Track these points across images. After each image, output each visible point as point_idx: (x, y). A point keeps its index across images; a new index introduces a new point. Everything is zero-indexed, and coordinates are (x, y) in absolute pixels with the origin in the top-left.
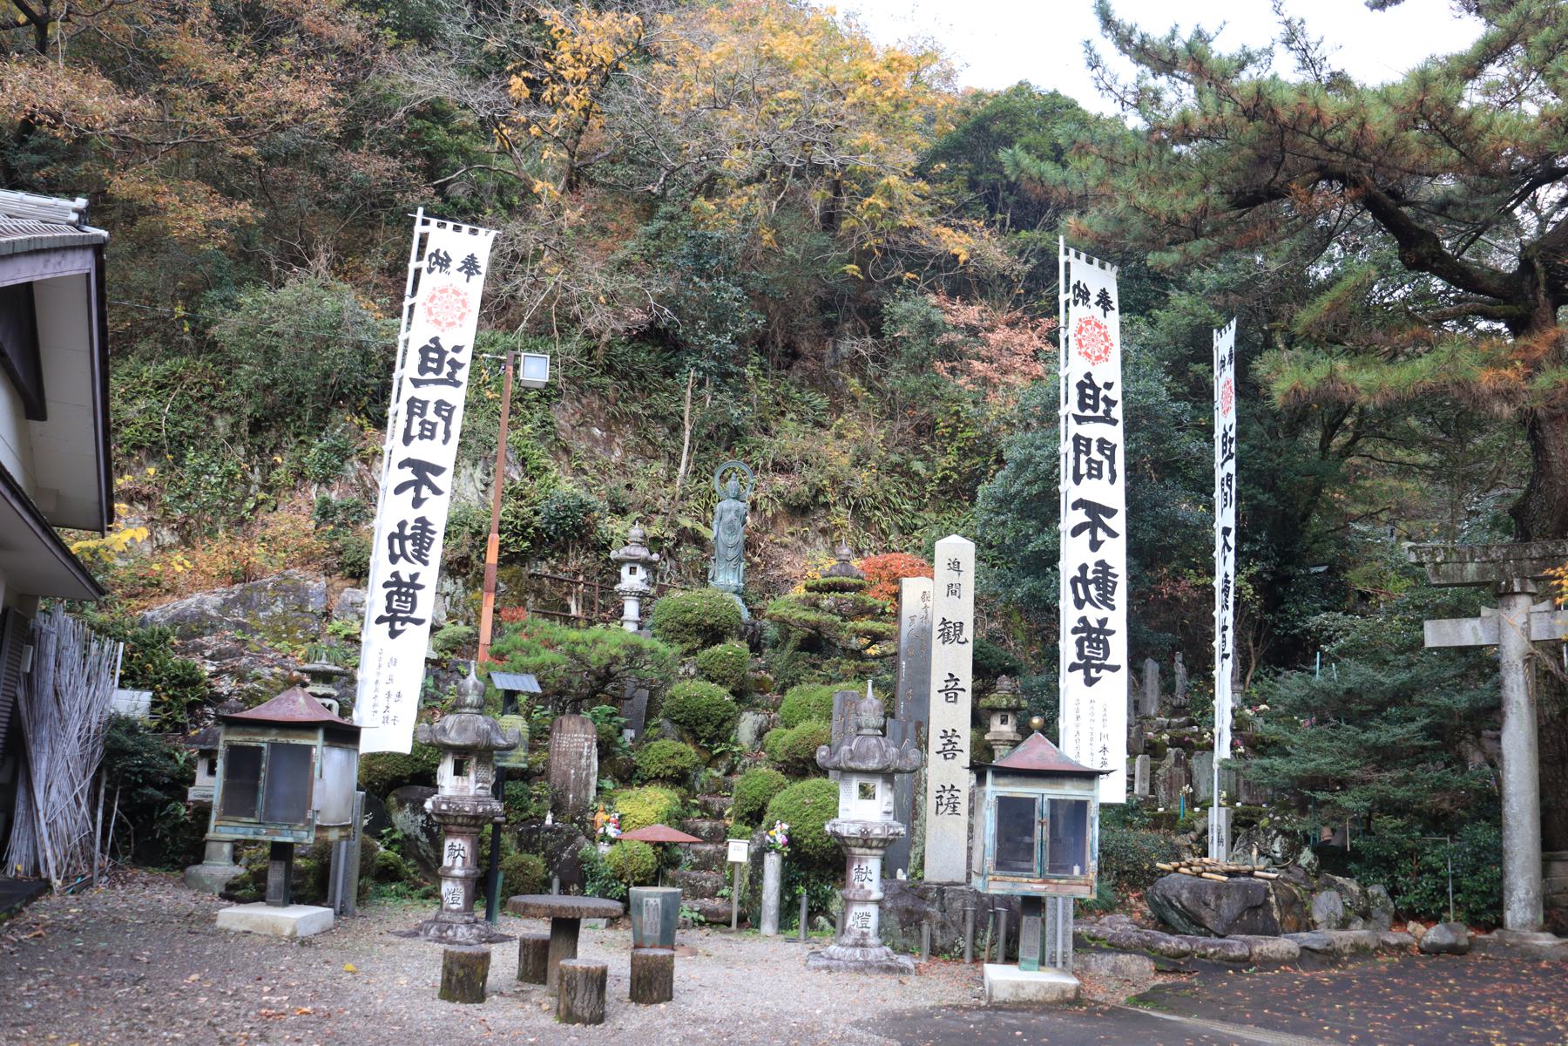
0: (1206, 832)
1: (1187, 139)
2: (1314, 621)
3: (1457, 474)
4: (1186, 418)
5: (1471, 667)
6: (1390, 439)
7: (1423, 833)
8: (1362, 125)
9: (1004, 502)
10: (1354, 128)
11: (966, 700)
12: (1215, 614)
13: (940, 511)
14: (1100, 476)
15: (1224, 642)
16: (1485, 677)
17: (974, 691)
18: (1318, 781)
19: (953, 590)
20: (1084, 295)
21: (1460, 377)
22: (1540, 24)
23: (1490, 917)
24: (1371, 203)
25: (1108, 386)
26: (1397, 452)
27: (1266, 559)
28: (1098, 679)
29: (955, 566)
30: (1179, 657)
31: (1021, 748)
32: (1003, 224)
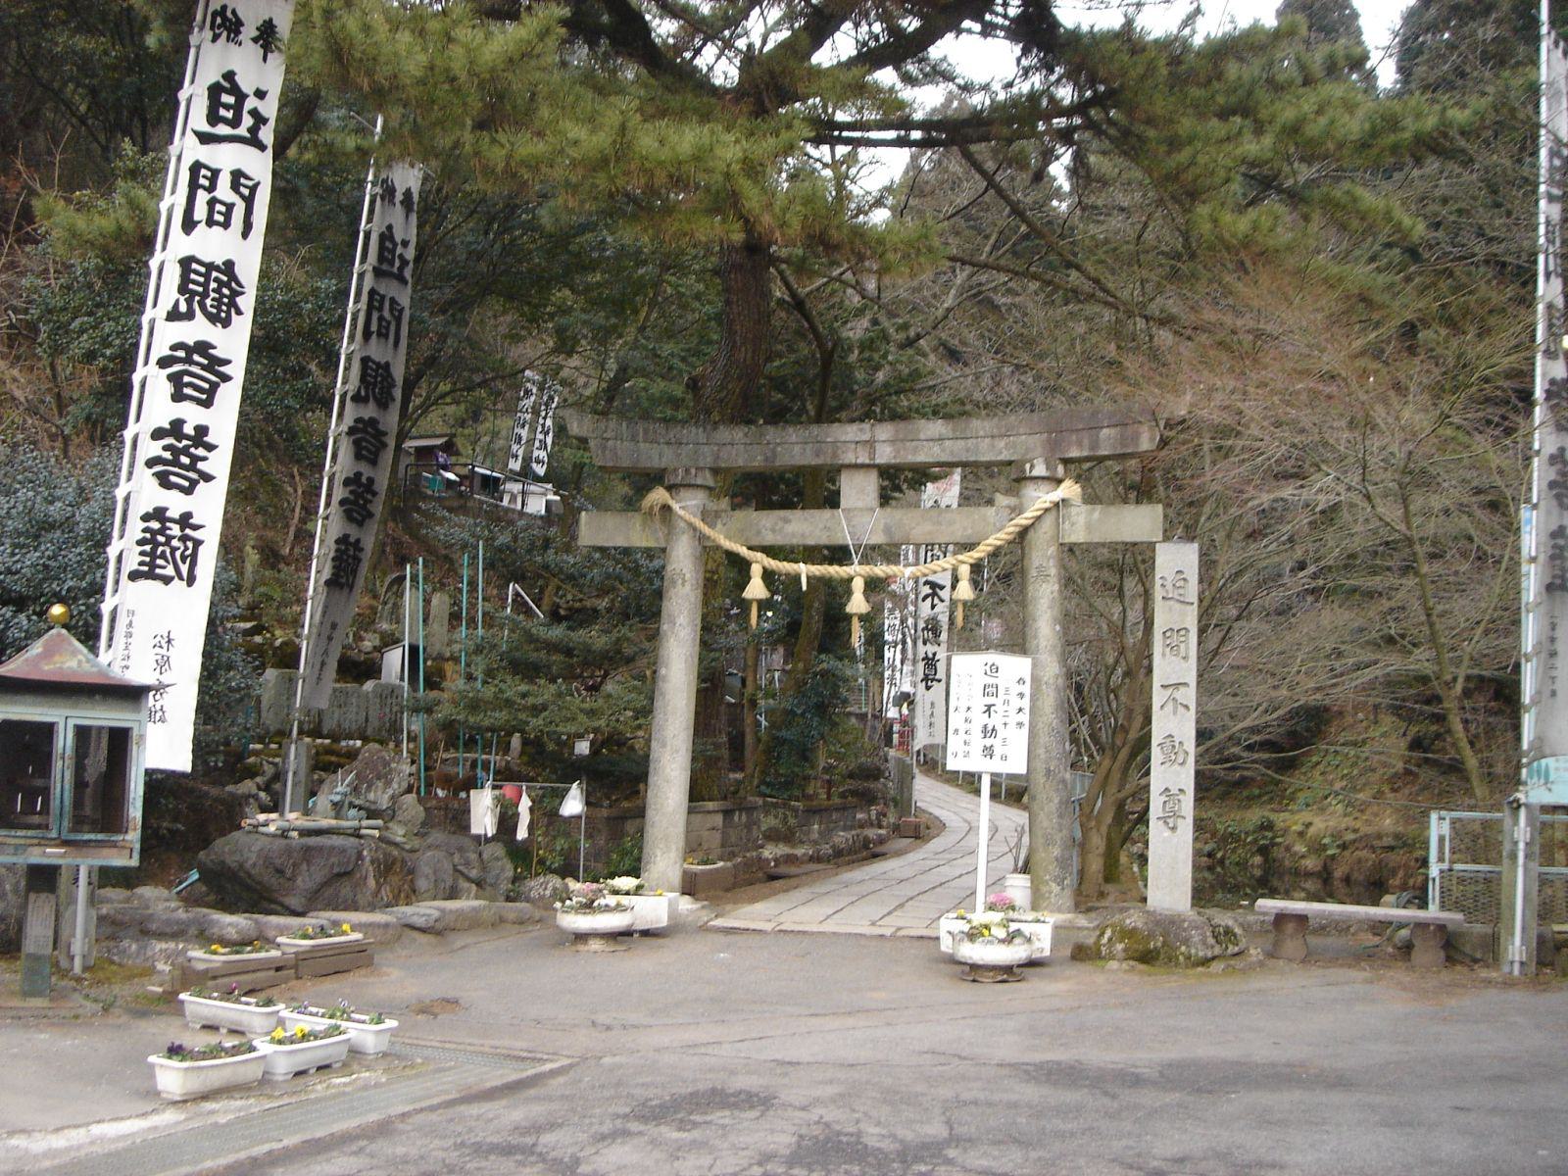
14: (226, 225)
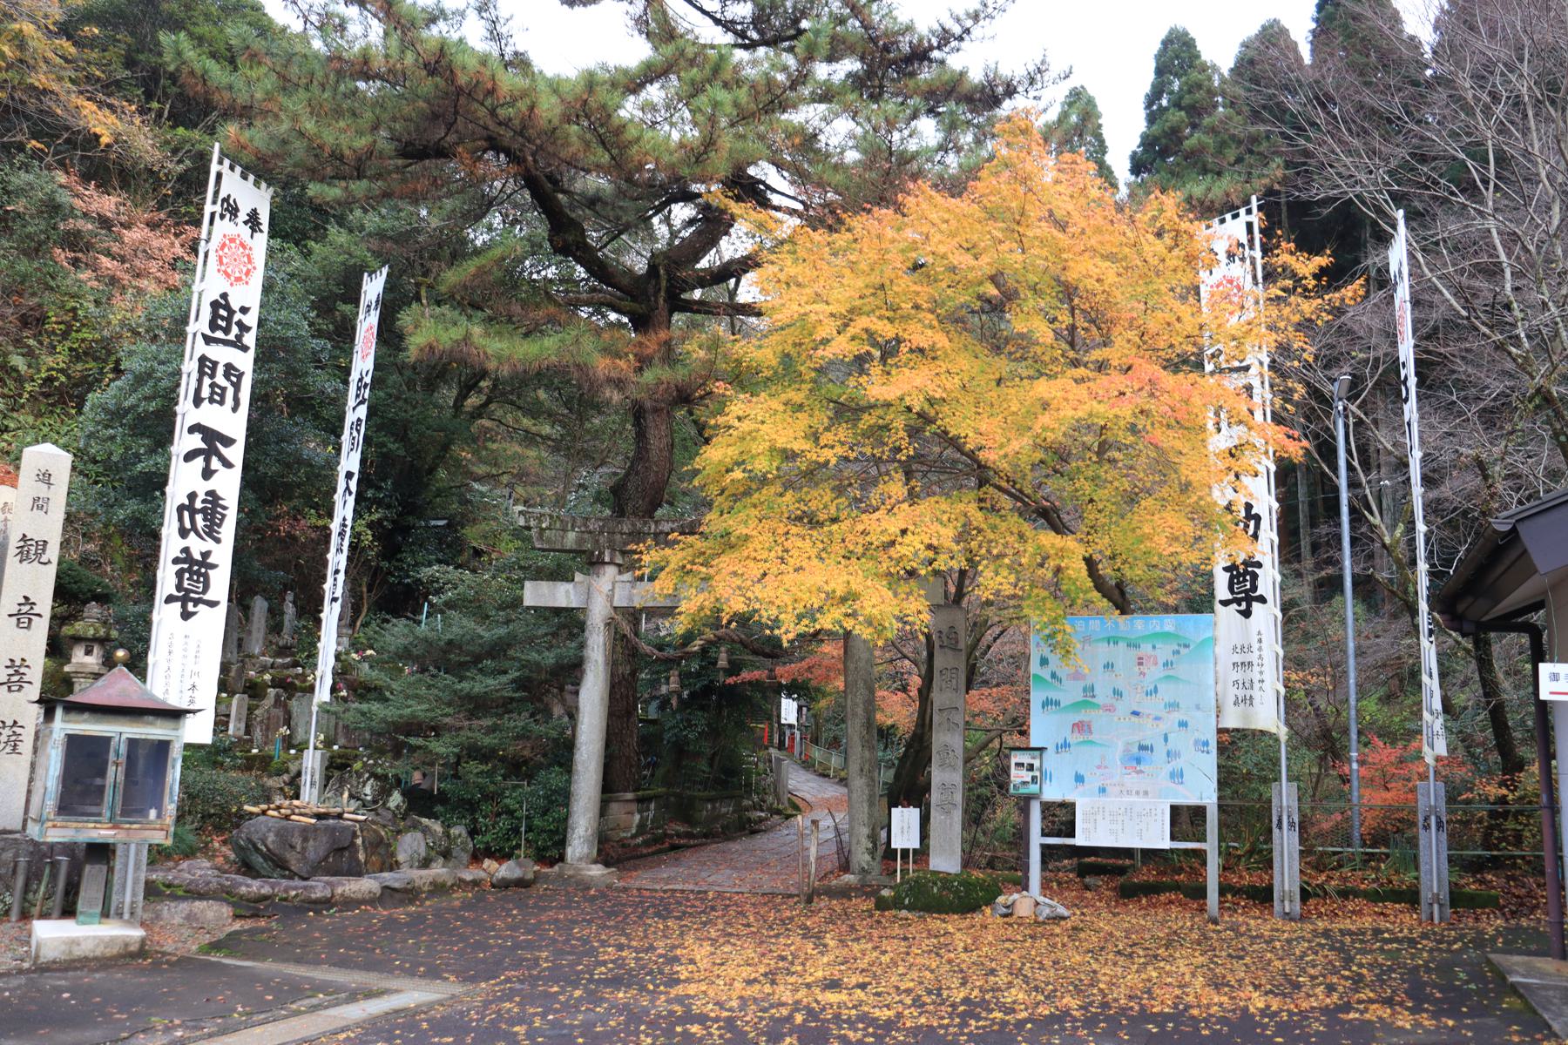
0: (299, 774)
1: (367, 77)
2: (425, 573)
3: (574, 450)
4: (324, 357)
5: (564, 626)
6: (519, 408)
7: (505, 778)
8: (532, 108)
9: (115, 415)
10: (524, 109)
11: (41, 628)
12: (329, 556)
13: (38, 415)
14: (221, 403)
15: (334, 586)
16: (572, 636)
17: (53, 618)
18: (413, 727)
19: (39, 504)
20: (232, 210)
21: (580, 360)
22: (692, 63)
23: (555, 853)
24: (531, 183)
25: (244, 310)
26: (525, 421)
27: (389, 507)
28: (194, 614)
29: (45, 478)
30: (290, 596)
31: (100, 682)
32: (160, 114)
